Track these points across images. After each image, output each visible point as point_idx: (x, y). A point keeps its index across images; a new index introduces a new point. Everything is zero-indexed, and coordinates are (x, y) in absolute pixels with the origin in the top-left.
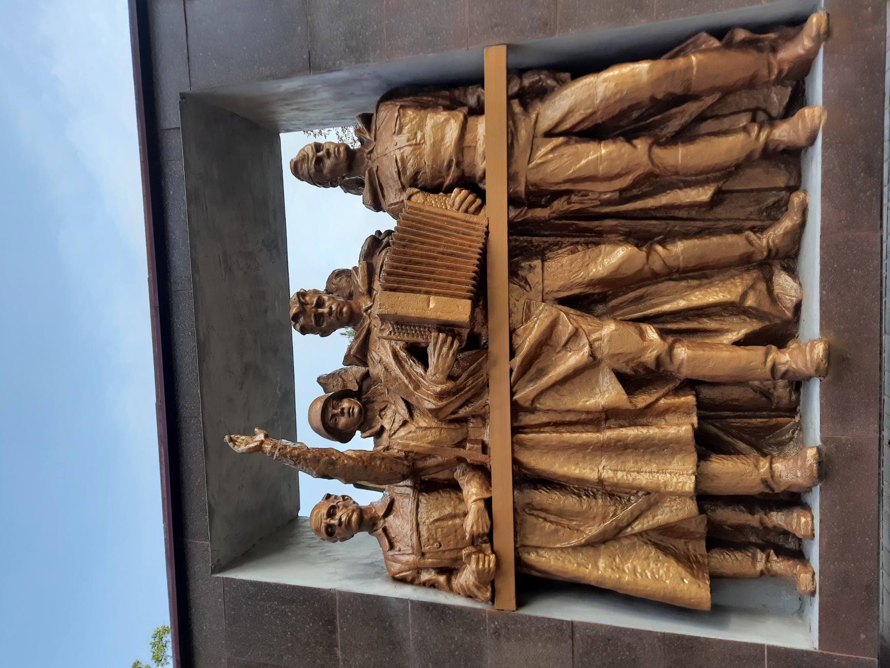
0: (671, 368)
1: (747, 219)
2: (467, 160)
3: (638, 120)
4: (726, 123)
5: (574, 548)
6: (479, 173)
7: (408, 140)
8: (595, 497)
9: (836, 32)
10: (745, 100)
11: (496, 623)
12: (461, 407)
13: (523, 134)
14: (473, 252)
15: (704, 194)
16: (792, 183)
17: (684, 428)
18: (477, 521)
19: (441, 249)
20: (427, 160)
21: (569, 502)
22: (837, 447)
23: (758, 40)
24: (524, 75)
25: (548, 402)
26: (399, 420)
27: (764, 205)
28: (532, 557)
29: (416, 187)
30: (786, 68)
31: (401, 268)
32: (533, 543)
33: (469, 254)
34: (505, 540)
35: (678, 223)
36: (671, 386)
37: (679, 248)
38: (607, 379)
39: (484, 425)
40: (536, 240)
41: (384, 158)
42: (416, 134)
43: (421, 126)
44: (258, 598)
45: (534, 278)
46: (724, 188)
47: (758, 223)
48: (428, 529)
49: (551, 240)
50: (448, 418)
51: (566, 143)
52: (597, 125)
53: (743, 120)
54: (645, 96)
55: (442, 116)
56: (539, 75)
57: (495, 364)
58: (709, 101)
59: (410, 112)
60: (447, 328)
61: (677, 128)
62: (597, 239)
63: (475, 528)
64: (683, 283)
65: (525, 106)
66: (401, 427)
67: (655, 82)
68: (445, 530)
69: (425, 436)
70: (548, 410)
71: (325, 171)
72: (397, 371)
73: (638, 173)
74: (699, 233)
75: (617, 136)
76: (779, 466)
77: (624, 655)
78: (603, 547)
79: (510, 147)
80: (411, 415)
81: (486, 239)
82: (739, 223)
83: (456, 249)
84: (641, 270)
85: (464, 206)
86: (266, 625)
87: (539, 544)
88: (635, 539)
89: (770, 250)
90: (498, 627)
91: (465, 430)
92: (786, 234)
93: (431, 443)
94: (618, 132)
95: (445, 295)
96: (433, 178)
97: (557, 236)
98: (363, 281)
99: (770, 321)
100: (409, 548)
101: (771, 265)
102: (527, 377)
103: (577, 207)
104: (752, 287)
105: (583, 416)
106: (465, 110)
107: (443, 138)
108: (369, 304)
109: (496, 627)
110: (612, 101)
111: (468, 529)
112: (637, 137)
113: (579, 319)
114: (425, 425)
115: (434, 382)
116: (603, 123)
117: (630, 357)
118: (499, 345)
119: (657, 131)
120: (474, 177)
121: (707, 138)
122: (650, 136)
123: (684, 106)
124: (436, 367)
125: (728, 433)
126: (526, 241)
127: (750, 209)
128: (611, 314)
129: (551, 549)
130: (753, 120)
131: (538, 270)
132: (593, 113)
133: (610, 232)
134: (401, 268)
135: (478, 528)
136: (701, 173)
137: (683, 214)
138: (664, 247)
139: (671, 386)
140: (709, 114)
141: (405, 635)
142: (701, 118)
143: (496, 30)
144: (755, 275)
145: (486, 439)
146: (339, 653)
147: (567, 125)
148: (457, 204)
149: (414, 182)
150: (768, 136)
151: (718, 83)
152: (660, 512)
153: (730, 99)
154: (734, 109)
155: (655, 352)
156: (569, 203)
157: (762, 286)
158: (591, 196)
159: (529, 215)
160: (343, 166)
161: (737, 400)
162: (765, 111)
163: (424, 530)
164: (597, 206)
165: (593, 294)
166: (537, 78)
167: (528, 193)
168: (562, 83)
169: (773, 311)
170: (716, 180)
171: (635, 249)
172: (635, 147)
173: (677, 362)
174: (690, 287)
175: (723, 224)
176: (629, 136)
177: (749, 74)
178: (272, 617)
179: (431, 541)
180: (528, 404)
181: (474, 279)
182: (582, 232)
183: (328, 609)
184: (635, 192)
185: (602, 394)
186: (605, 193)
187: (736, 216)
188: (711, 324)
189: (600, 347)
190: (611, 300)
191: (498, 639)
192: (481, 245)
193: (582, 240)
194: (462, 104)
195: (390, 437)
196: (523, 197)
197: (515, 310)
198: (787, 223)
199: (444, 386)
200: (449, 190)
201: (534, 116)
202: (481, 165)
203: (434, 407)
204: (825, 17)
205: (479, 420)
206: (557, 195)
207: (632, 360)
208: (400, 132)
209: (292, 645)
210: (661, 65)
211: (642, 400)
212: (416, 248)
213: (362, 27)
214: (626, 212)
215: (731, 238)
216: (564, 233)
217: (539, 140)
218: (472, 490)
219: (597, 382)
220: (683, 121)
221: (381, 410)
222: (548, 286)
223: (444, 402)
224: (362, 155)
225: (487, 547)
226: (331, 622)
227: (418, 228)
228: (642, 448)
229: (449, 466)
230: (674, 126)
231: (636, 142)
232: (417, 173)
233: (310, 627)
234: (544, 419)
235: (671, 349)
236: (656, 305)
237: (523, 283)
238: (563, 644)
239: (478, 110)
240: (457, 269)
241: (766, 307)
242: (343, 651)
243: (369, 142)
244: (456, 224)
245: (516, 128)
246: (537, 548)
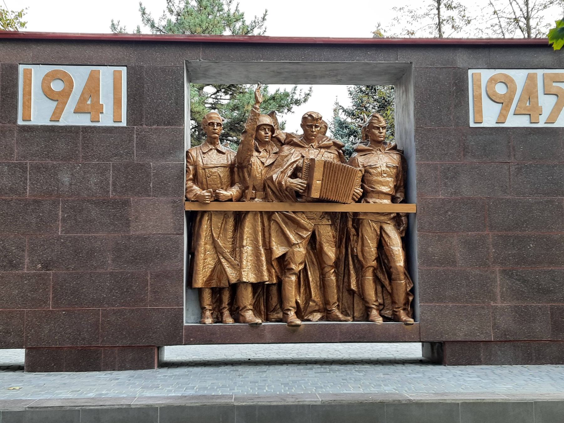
0: (288, 274)
1: (342, 304)
2: (374, 195)
3: (384, 262)
4: (380, 295)
5: (212, 235)
6: (369, 200)
7: (383, 171)
8: (233, 244)
9: (407, 327)
10: (388, 301)
12: (271, 190)
13: (382, 218)
14: (337, 198)
15: (353, 286)
16: (355, 318)
17: (267, 278)
18: (224, 196)
19: (339, 185)
20: (375, 178)
21: (230, 234)
22: (262, 330)
23: (408, 304)
24: (406, 217)
25: (273, 226)
26: (263, 160)
27: (347, 309)
28: (206, 218)
29: (365, 172)
30: (397, 313)
31: (333, 169)
32: (213, 218)
33: (337, 197)
34: (214, 207)
35: (342, 278)
36: (279, 274)
37: (333, 278)
38: (283, 250)
39: (262, 199)
40: (339, 221)
41: (377, 158)
42: (386, 174)
43: (389, 176)
45: (325, 221)
46: (355, 294)
47: (340, 308)
49: (338, 227)
50: (266, 183)
51: (377, 235)
52: (383, 247)
53: (380, 301)
54: (392, 265)
55: (392, 185)
56: (405, 224)
57: (291, 205)
58: (389, 288)
59: (395, 171)
60: (309, 188)
61: (379, 277)
62: (337, 246)
63: (222, 195)
64: (318, 280)
65: (394, 218)
66: (261, 162)
67: (396, 268)
68: (216, 180)
69: (258, 173)
70: (270, 226)
71: (373, 130)
72: (289, 163)
73: (364, 262)
74: (338, 286)
75: (378, 254)
76: (250, 312)
78: (212, 247)
79: (378, 213)
80: (266, 166)
81: (342, 203)
82: (341, 301)
83: (339, 191)
84: (325, 264)
85: (356, 194)
87: (213, 221)
88: (217, 260)
89: (330, 311)
91: (260, 190)
92: (337, 316)
93: (256, 175)
94: (380, 255)
95: (322, 187)
96: (368, 180)
97: (340, 229)
98: (325, 144)
99: (303, 311)
101: (324, 312)
102: (284, 218)
103: (352, 239)
104: (317, 305)
105: (267, 240)
106: (394, 194)
107: (384, 186)
108: (315, 147)
110: (391, 253)
111: (221, 192)
112: (377, 262)
113: (307, 239)
114: (263, 173)
115: (286, 181)
116: (384, 249)
117: (293, 259)
118: (298, 207)
119: (379, 269)
120: (367, 197)
121: (375, 287)
122: (377, 267)
123: (387, 279)
124: (292, 183)
125: (258, 296)
126: (338, 217)
127: (346, 304)
128: (308, 252)
129: (211, 225)
130: (380, 304)
131: (328, 223)
132: (387, 245)
133: (340, 251)
134: (333, 169)
135: (222, 196)
136: (362, 286)
137: (346, 280)
138: (333, 272)
139: (279, 274)
140: (384, 289)
141: (168, 160)
142: (383, 286)
144: (321, 306)
145: (256, 199)
146: (155, 127)
147: (384, 235)
148: (356, 191)
149: (366, 171)
150: (373, 308)
151: (395, 291)
152: (230, 269)
153: (389, 296)
154: (385, 298)
155: (294, 268)
156: (353, 235)
157: (317, 308)
158: (356, 244)
159: (349, 219)
160: (375, 139)
161: (272, 299)
162: (383, 309)
163: (214, 170)
164: (351, 246)
165: (315, 244)
166: (404, 223)
167: (359, 219)
168: (401, 233)
169: (307, 312)
170: (359, 291)
171: (334, 261)
172: (374, 261)
173: (290, 276)
174: (317, 282)
175: (341, 295)
176: (378, 259)
177: (397, 302)
179: (210, 173)
180: (273, 218)
181: (327, 199)
182: (340, 240)
183: (175, 122)
184: (356, 261)
185: (277, 248)
186: (357, 250)
187: (344, 300)
188: (302, 290)
189: (297, 247)
190: (312, 251)
191: (172, 202)
192: (340, 201)
193: (337, 240)
194: (396, 192)
195: (257, 156)
197: (312, 213)
198: (341, 316)
199: (284, 186)
200: (362, 187)
201: (389, 222)
202: (371, 201)
203: (274, 180)
204: (412, 323)
205: (264, 196)
206: (357, 230)
207: (291, 260)
208: (387, 167)
210: (402, 270)
211: (275, 264)
212: (340, 175)
214: (348, 258)
215: (336, 297)
216: (341, 232)
217: (379, 224)
218: (234, 191)
219: (282, 246)
220: (382, 279)
221: (266, 150)
222: (321, 227)
223: (277, 185)
224: (379, 146)
225: (213, 199)
226: (169, 124)
227: (348, 175)
228: (257, 263)
229: (243, 181)
230: (381, 276)
231: (375, 261)
232: (370, 173)
234: (266, 224)
235: (295, 274)
236: (310, 269)
237: (322, 216)
238: (173, 230)
239: (394, 200)
240: (331, 192)
241: (309, 310)
242: (156, 129)
243: (385, 150)
244: (348, 191)
245: (385, 215)
246: (211, 219)
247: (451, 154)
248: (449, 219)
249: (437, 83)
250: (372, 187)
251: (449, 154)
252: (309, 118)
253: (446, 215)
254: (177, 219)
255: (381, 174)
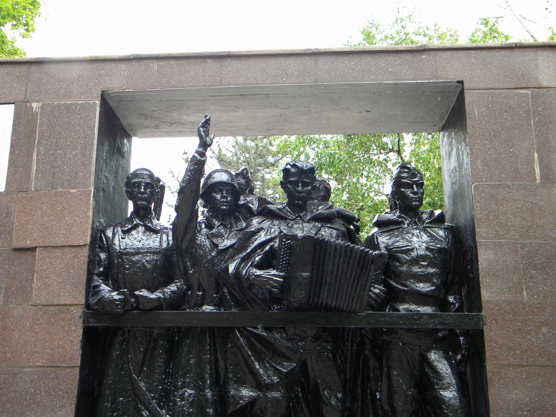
2: (407, 298)
11: (74, 311)
44: (85, 128)
48: (139, 261)
77: (57, 403)
86: (65, 133)
90: (72, 313)
100: (125, 246)
109: (72, 311)
143: (493, 322)
178: (71, 139)
196: (230, 411)
209: (51, 154)
213: (502, 224)
233: (65, 169)
247: (538, 226)
248: (544, 341)
249: (506, 111)
250: (405, 286)
251: (535, 227)
252: (293, 170)
253: (538, 334)
254: (71, 341)
255: (416, 261)
